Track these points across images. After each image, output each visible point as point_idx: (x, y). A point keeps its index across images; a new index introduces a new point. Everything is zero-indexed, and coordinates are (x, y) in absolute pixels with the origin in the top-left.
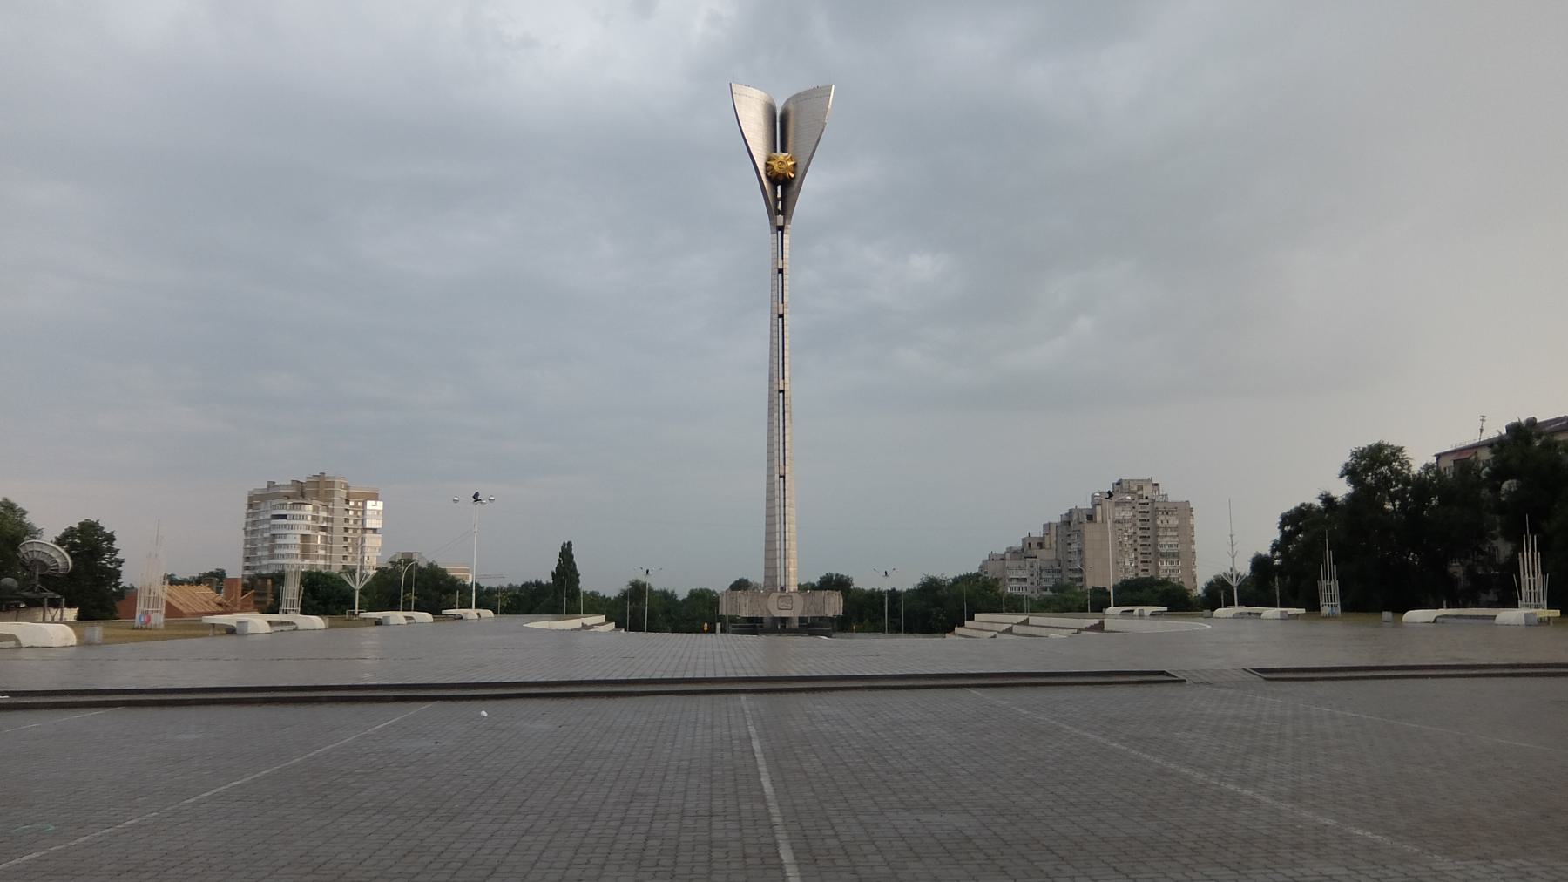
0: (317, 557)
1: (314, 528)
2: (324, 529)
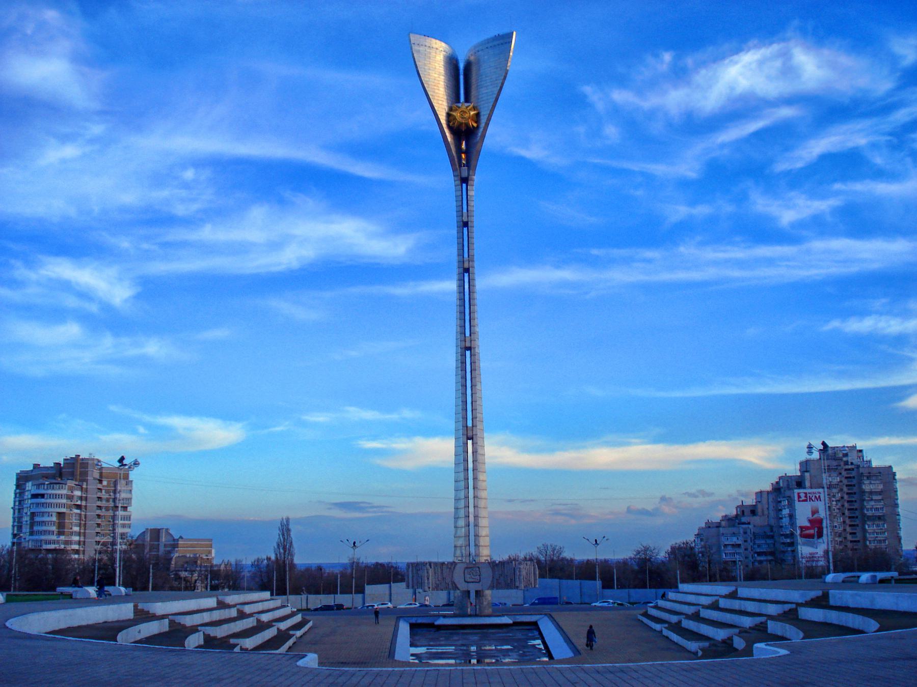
0: (72, 534)
1: (70, 507)
2: (79, 507)
